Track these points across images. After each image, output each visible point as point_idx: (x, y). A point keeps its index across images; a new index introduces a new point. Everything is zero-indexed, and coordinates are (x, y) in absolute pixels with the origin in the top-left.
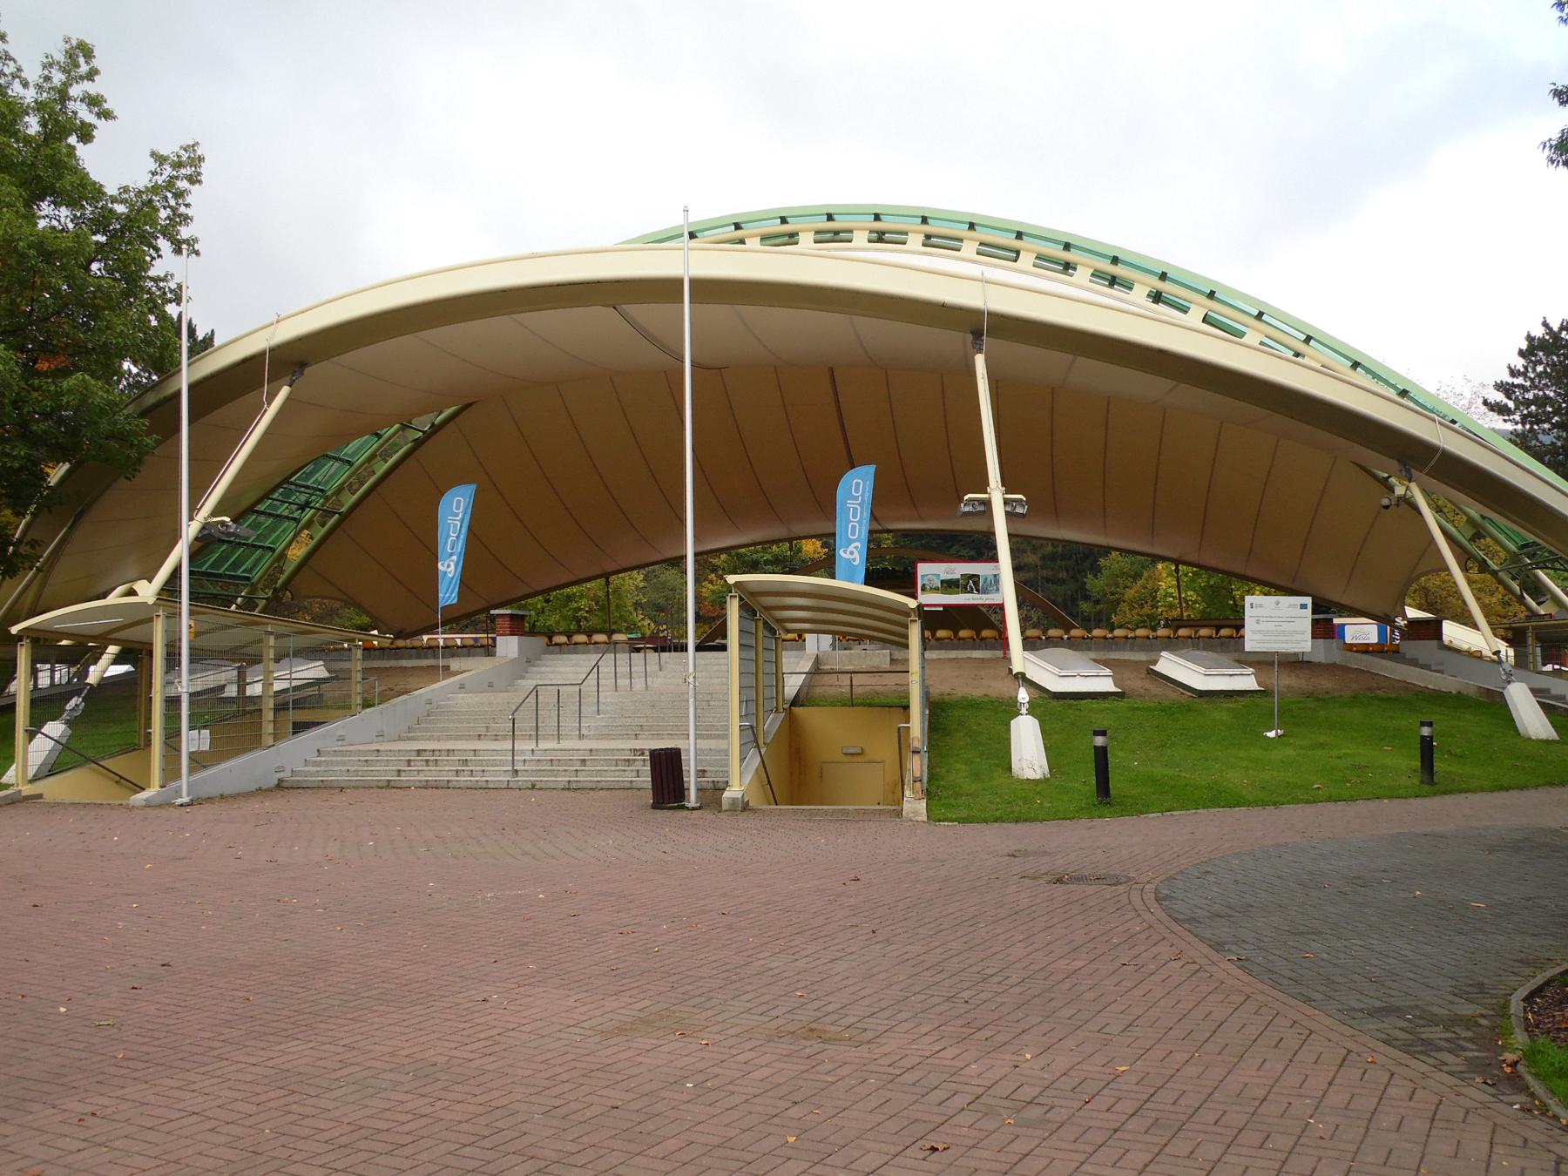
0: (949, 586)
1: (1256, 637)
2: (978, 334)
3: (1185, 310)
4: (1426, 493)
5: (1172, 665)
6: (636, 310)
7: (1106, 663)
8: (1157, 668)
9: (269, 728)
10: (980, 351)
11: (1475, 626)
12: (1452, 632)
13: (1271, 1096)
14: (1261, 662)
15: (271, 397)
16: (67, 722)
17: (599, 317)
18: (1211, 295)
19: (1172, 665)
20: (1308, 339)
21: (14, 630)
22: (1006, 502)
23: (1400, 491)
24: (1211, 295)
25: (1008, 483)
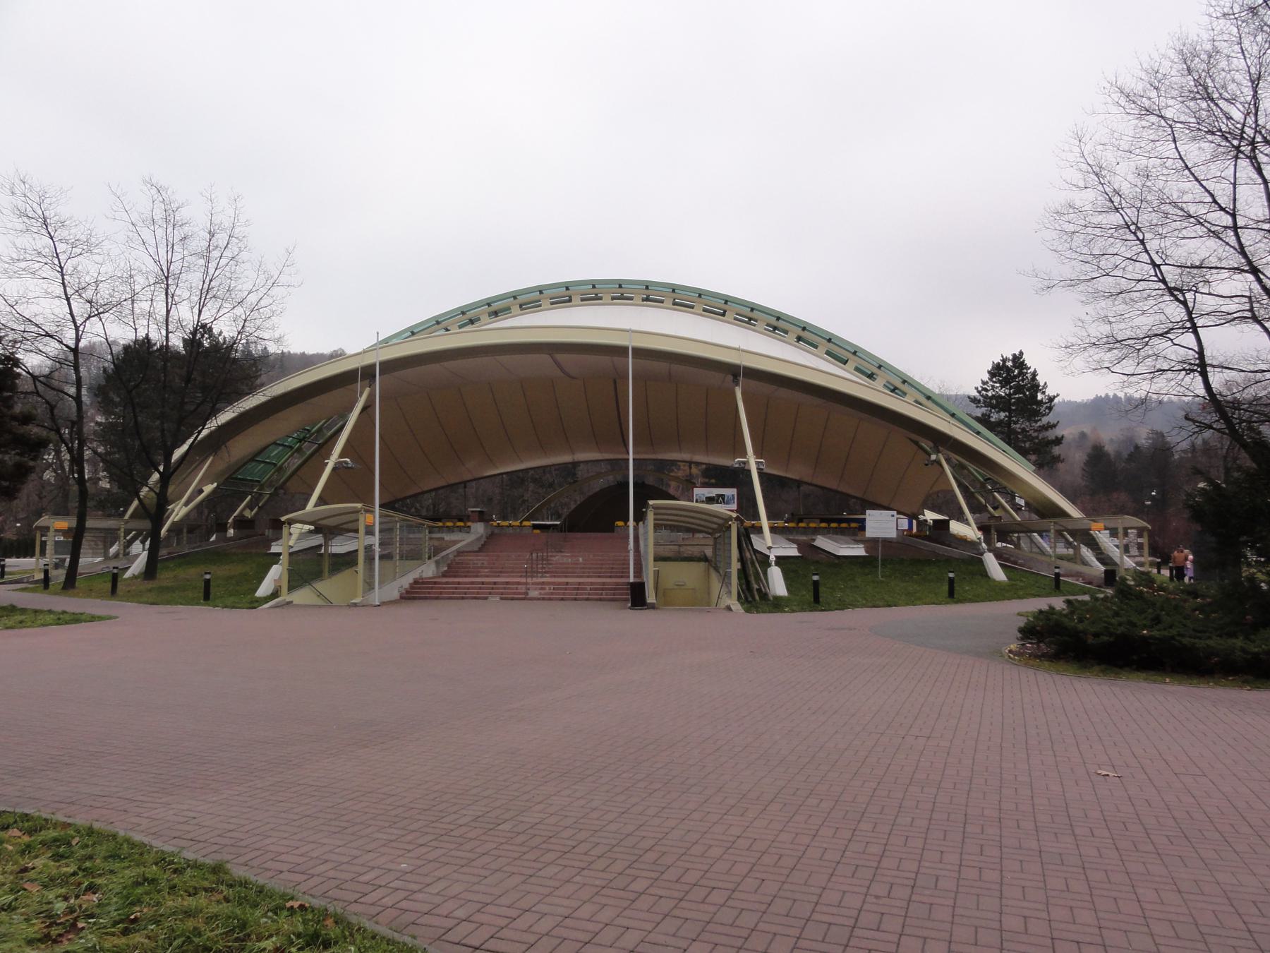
0: (710, 500)
1: (870, 532)
2: (736, 376)
3: (816, 347)
4: (948, 460)
5: (823, 542)
6: (561, 357)
7: (793, 541)
8: (815, 543)
9: (326, 570)
10: (737, 384)
11: (968, 524)
12: (956, 527)
13: (799, 866)
14: (872, 543)
15: (362, 394)
16: (1106, 571)
17: (544, 358)
18: (829, 340)
19: (823, 542)
20: (880, 367)
21: (283, 519)
22: (757, 463)
23: (933, 457)
24: (829, 340)
25: (758, 453)
